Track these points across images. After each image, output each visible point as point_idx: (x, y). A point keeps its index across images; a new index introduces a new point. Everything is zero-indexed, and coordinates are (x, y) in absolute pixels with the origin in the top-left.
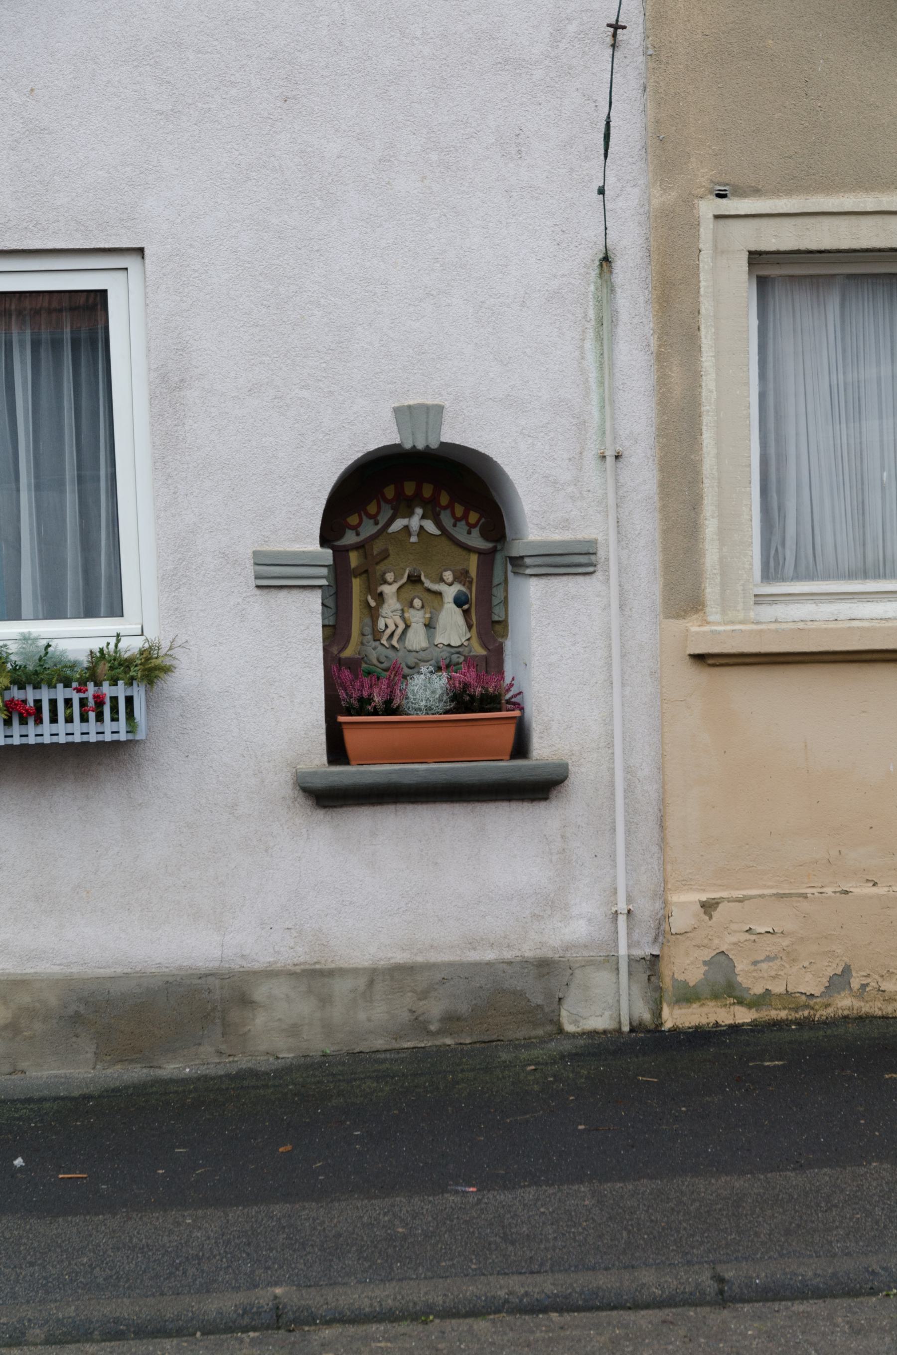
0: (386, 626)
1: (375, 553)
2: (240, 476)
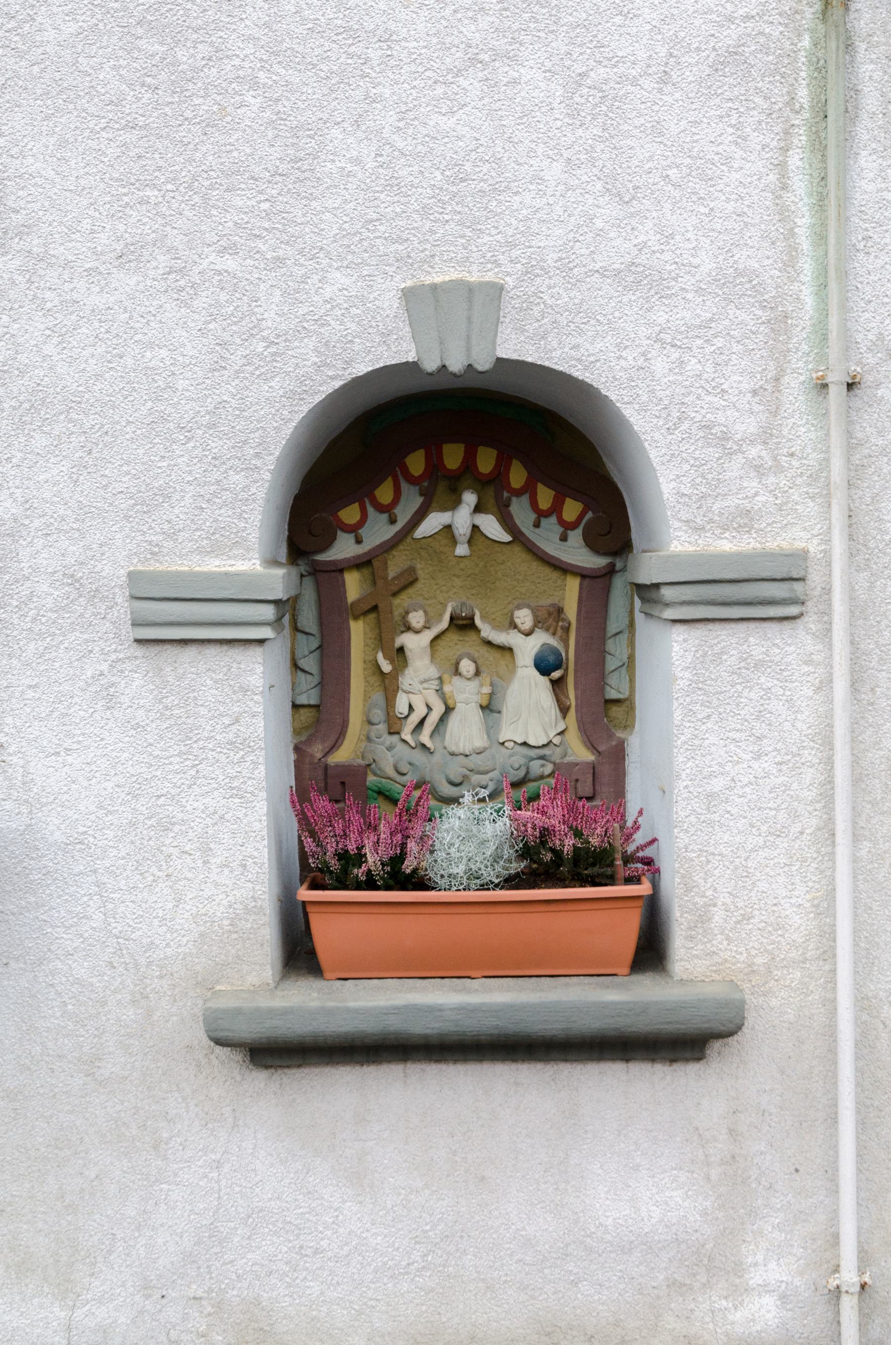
0: (411, 708)
1: (391, 574)
2: (103, 426)
